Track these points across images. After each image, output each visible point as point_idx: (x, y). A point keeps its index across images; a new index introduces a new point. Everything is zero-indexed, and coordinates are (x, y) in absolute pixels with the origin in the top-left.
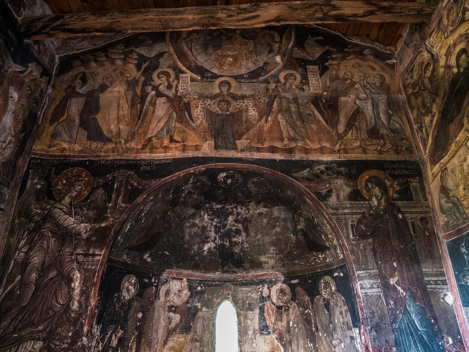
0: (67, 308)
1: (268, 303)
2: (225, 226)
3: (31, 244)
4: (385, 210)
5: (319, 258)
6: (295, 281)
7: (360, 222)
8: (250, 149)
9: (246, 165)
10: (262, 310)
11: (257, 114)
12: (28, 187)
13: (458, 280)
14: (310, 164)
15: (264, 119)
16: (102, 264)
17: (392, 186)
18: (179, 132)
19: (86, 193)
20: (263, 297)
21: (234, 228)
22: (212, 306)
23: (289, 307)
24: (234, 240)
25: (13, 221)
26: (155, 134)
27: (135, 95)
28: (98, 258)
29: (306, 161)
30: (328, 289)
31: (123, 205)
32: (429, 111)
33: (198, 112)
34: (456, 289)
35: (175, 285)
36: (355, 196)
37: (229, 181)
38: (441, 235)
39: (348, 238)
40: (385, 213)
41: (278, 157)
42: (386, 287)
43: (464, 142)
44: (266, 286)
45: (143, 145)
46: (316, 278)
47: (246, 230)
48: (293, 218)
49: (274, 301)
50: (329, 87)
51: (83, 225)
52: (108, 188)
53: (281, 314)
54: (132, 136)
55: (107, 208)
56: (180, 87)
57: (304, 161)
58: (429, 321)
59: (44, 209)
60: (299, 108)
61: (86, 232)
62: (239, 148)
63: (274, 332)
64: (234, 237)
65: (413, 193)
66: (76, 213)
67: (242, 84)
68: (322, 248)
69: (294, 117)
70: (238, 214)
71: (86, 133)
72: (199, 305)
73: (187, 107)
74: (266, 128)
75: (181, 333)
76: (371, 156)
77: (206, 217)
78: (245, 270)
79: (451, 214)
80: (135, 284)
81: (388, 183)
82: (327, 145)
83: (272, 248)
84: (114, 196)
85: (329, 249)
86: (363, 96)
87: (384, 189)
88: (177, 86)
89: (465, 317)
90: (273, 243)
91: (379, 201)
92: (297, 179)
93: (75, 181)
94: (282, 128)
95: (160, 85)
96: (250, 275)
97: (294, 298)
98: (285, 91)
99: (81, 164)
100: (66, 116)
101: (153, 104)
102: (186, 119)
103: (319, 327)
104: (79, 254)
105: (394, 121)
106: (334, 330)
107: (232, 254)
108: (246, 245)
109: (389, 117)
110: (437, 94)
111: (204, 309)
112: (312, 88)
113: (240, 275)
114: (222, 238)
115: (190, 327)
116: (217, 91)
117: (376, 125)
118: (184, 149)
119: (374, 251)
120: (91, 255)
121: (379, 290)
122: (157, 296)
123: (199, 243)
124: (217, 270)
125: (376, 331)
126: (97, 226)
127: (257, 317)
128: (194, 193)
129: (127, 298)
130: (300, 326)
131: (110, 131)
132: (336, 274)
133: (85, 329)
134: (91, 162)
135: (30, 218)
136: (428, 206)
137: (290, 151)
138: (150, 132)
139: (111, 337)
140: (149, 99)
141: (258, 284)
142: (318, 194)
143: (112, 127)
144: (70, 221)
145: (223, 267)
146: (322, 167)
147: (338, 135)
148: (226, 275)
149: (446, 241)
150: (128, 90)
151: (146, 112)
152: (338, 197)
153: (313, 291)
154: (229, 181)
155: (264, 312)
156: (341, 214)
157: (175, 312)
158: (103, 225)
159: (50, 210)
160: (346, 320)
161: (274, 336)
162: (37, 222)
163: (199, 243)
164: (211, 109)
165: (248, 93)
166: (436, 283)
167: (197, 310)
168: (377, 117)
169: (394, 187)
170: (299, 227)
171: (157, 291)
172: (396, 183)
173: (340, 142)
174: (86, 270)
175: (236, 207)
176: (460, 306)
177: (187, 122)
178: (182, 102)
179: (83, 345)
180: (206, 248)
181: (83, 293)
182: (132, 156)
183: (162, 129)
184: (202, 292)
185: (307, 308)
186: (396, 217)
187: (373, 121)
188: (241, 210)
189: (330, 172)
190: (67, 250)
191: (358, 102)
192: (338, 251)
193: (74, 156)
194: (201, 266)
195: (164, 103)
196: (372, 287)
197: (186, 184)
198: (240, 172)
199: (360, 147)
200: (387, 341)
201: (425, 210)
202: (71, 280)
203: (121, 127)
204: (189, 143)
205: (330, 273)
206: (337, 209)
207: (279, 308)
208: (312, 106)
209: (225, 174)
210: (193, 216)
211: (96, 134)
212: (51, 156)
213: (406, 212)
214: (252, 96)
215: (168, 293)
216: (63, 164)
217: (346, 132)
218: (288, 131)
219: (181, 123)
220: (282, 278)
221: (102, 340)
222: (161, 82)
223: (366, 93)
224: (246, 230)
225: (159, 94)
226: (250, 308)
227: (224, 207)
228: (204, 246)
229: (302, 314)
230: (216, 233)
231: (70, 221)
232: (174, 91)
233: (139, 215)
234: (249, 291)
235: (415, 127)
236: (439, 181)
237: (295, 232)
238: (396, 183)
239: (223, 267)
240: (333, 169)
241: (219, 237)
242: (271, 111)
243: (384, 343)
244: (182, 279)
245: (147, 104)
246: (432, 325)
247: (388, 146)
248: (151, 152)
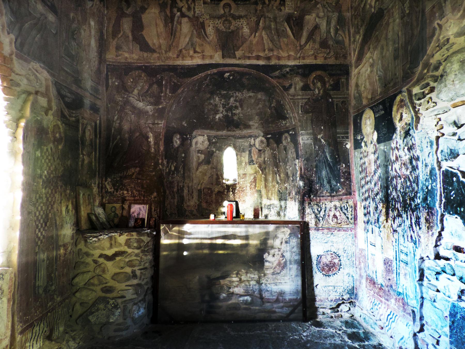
0: (148, 151)
1: (253, 148)
2: (228, 104)
4: (322, 97)
5: (283, 123)
6: (269, 136)
7: (306, 103)
8: (244, 57)
9: (241, 69)
10: (250, 152)
11: (249, 31)
12: (110, 84)
13: (354, 137)
14: (281, 67)
15: (253, 35)
16: (163, 129)
17: (329, 81)
18: (199, 45)
19: (147, 87)
20: (251, 145)
21: (234, 105)
22: (221, 150)
23: (265, 150)
24: (234, 112)
25: (107, 105)
26: (183, 47)
27: (166, 16)
28: (161, 125)
29: (278, 65)
30: (286, 140)
31: (170, 95)
32: (359, 33)
33: (210, 30)
34: (353, 141)
35: (200, 139)
36: (306, 88)
37: (231, 78)
39: (298, 113)
40: (322, 98)
41: (261, 63)
42: (316, 140)
44: (253, 139)
45: (177, 55)
46: (281, 134)
47: (241, 106)
48: (269, 100)
49: (257, 147)
50: (299, 7)
51: (148, 107)
52: (160, 84)
53: (261, 154)
54: (169, 48)
55: (161, 96)
56: (196, 9)
57: (277, 65)
58: (335, 156)
59: (124, 98)
60: (277, 26)
61: (151, 111)
62: (237, 57)
63: (257, 163)
64: (234, 110)
65: (341, 85)
66: (143, 100)
67: (239, 6)
68: (285, 118)
69: (273, 32)
70: (237, 97)
71: (139, 46)
72: (214, 150)
73: (203, 26)
74: (254, 42)
75: (205, 164)
76: (320, 61)
77: (217, 99)
78: (241, 129)
80: (179, 138)
81: (327, 79)
82: (292, 53)
83: (257, 117)
84: (164, 89)
85: (288, 118)
86: (321, 14)
87: (324, 83)
88: (194, 8)
90: (257, 114)
91: (319, 91)
92: (272, 77)
93: (138, 79)
94: (265, 42)
95: (183, 7)
96: (243, 132)
97: (268, 145)
98: (268, 12)
99: (139, 68)
100: (122, 32)
101: (180, 23)
102: (203, 35)
103: (281, 160)
104: (150, 124)
105: (340, 34)
106: (288, 161)
107: (233, 120)
108: (241, 115)
109: (336, 31)
110: (363, 22)
111: (217, 152)
112: (287, 8)
113: (238, 132)
114: (227, 111)
115: (210, 161)
116: (222, 12)
117: (326, 38)
118: (203, 57)
119: (312, 121)
120: (157, 124)
121: (312, 141)
122: (191, 145)
123: (213, 114)
124: (224, 130)
125: (307, 161)
126: (157, 107)
127: (247, 156)
128: (210, 85)
129: (176, 146)
130: (271, 160)
131: (154, 44)
132: (291, 133)
133: (160, 161)
134: (145, 66)
135: (117, 103)
136: (348, 94)
137: (269, 58)
138: (180, 45)
139: (171, 166)
140: (176, 19)
141: (248, 138)
142: (284, 87)
143: (155, 41)
144: (141, 105)
145: (228, 128)
146: (288, 69)
147: (301, 46)
148: (230, 133)
150: (161, 12)
151: (176, 30)
152: (295, 88)
153: (278, 141)
154: (231, 78)
155: (251, 153)
156: (296, 99)
157: (201, 153)
158: (160, 107)
159: (127, 98)
160: (293, 156)
161: (257, 166)
162: (121, 106)
163: (213, 114)
164: (219, 28)
165: (243, 14)
166: (343, 137)
167: (213, 152)
168: (328, 32)
169: (330, 82)
170: (272, 105)
171: (191, 142)
172: (331, 79)
173: (300, 52)
174: (155, 132)
175: (235, 93)
177: (204, 37)
178: (199, 23)
179: (160, 169)
180: (217, 117)
181: (155, 144)
182: (171, 63)
183: (188, 43)
184: (215, 143)
185: (275, 150)
186: (328, 101)
187: (325, 35)
188: (238, 94)
189: (292, 73)
190: (142, 121)
191: (317, 20)
192: (293, 120)
193: (134, 63)
194: (215, 127)
195: (187, 22)
196: (308, 139)
197: (206, 80)
198: (238, 72)
199: (313, 54)
200: (311, 165)
201: (346, 96)
202: (148, 138)
203: (161, 41)
204: (207, 53)
205: (288, 132)
206: (294, 96)
207: (260, 151)
208: (286, 24)
209: (229, 74)
210: (209, 99)
211: (145, 47)
212: (119, 63)
213: (334, 98)
214: (246, 16)
215: (196, 143)
216: (127, 69)
217: (306, 43)
218: (268, 43)
219: (200, 38)
220: (262, 134)
221: (168, 167)
222: (183, 5)
223: (324, 12)
224: (241, 106)
225: (183, 15)
226: (244, 151)
227: (228, 93)
228: (216, 116)
229: (272, 153)
230: (223, 108)
231: (141, 105)
232: (192, 13)
233: (179, 100)
234: (243, 142)
235: (352, 39)
237: (270, 108)
238: (331, 79)
239: (228, 128)
240: (295, 70)
241: (225, 110)
242: (258, 28)
243: (310, 166)
244: (204, 135)
245: (175, 23)
246: (336, 158)
247: (332, 53)
248: (183, 60)
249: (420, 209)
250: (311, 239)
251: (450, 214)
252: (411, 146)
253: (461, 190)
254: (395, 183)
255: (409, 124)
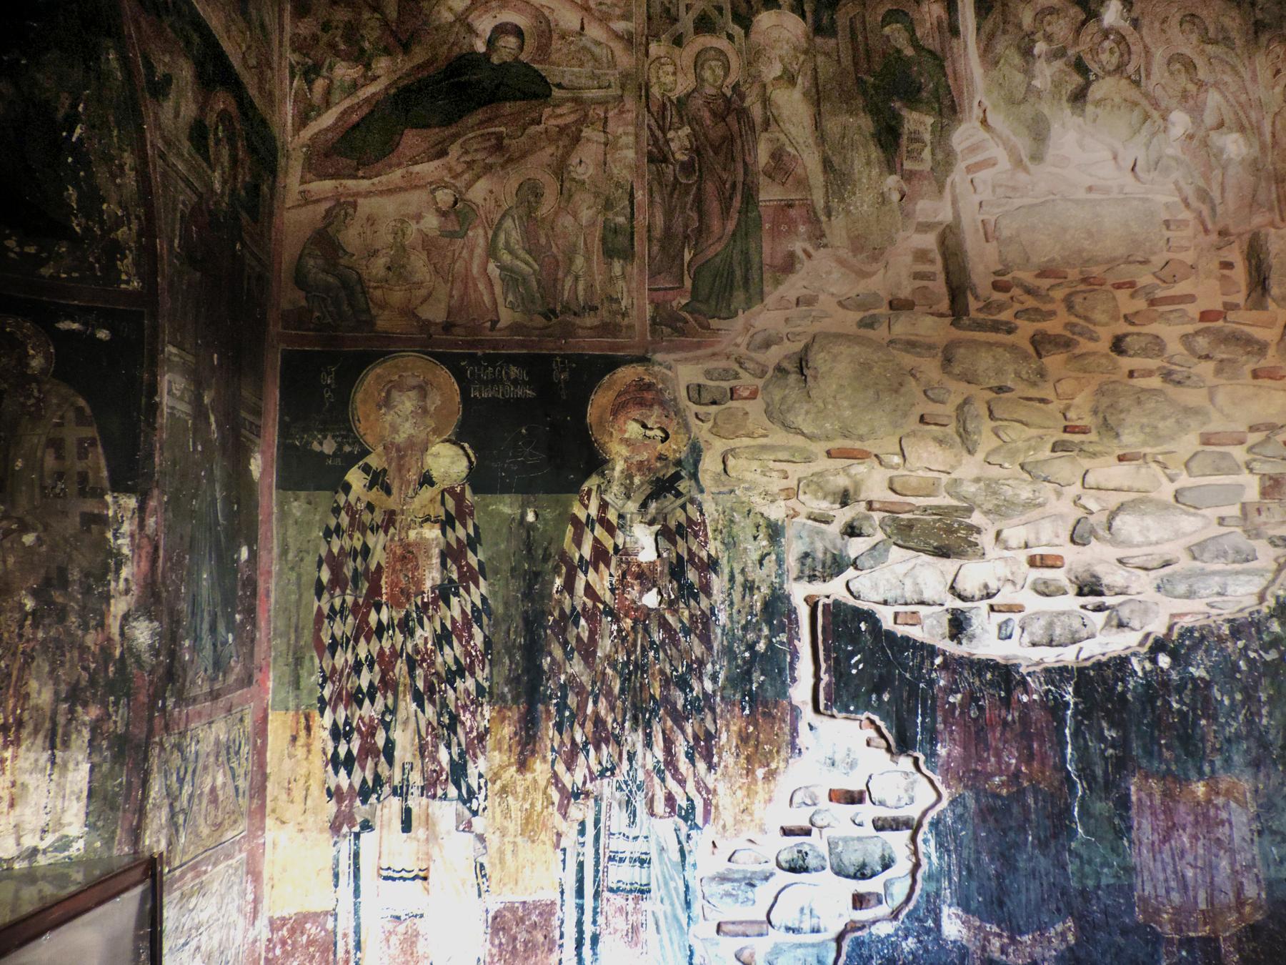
3: (356, 570)
13: (285, 431)
38: (275, 329)
43: (431, 183)
79: (324, 299)
89: (275, 510)
149: (282, 346)
176: (270, 487)
236: (319, 217)
249: (713, 710)
250: (165, 951)
251: (848, 711)
252: (680, 525)
253: (885, 653)
254: (585, 636)
255: (679, 463)
